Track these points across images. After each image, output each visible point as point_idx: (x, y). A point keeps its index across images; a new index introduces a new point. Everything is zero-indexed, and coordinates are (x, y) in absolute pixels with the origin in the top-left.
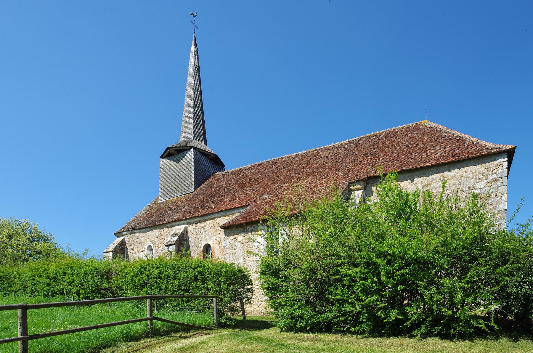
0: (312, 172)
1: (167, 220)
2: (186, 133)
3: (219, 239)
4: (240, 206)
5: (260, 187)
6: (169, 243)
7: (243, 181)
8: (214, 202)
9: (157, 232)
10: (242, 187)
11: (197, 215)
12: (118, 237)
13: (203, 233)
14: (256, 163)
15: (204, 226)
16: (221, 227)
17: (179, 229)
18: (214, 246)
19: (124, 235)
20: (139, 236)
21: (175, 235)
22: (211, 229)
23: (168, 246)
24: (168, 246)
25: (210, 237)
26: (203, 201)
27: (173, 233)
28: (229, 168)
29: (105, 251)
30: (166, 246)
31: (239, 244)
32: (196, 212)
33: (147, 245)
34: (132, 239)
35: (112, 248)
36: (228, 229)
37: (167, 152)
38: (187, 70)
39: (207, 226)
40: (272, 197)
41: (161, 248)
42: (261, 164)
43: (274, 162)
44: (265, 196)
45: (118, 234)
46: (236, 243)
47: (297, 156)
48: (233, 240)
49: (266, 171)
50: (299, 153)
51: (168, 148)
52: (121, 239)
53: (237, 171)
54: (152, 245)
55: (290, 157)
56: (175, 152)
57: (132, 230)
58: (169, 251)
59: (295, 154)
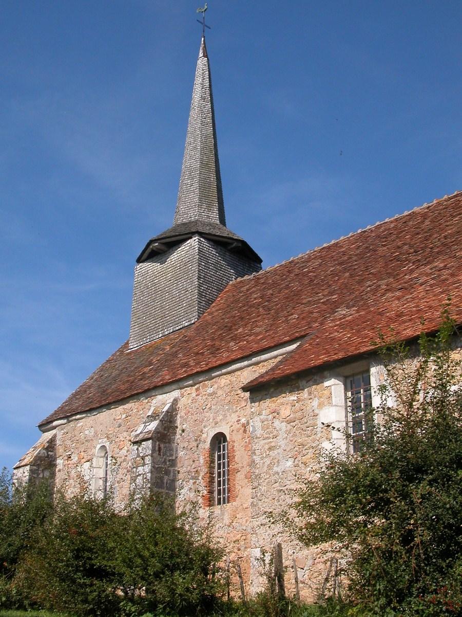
0: (444, 245)
1: (146, 384)
2: (190, 207)
3: (243, 420)
4: (287, 338)
5: (331, 294)
6: (141, 437)
7: (295, 286)
8: (234, 339)
9: (118, 412)
10: (294, 298)
11: (199, 369)
12: (44, 432)
13: (210, 408)
14: (325, 245)
15: (214, 393)
16: (245, 389)
17: (162, 401)
18: (235, 438)
19: (54, 428)
20: (87, 425)
21: (153, 417)
22: (229, 398)
23: (137, 443)
24: (137, 443)
25: (225, 416)
26: (213, 339)
27: (150, 414)
28: (268, 266)
29: (17, 464)
30: (135, 443)
31: (284, 424)
32: (198, 363)
33: (99, 446)
34: (69, 435)
35: (29, 459)
36: (259, 390)
37: (149, 251)
38: (190, 98)
39: (220, 392)
40: (358, 311)
41: (124, 452)
42: (336, 245)
43: (364, 236)
44: (342, 311)
45: (45, 426)
46: (277, 423)
47: (412, 216)
48: (271, 417)
49: (346, 258)
50: (416, 209)
51: (151, 242)
52: (48, 435)
53: (285, 266)
54: (107, 445)
55: (396, 220)
56: (163, 248)
57: (68, 413)
58: (138, 456)
59: (406, 213)
